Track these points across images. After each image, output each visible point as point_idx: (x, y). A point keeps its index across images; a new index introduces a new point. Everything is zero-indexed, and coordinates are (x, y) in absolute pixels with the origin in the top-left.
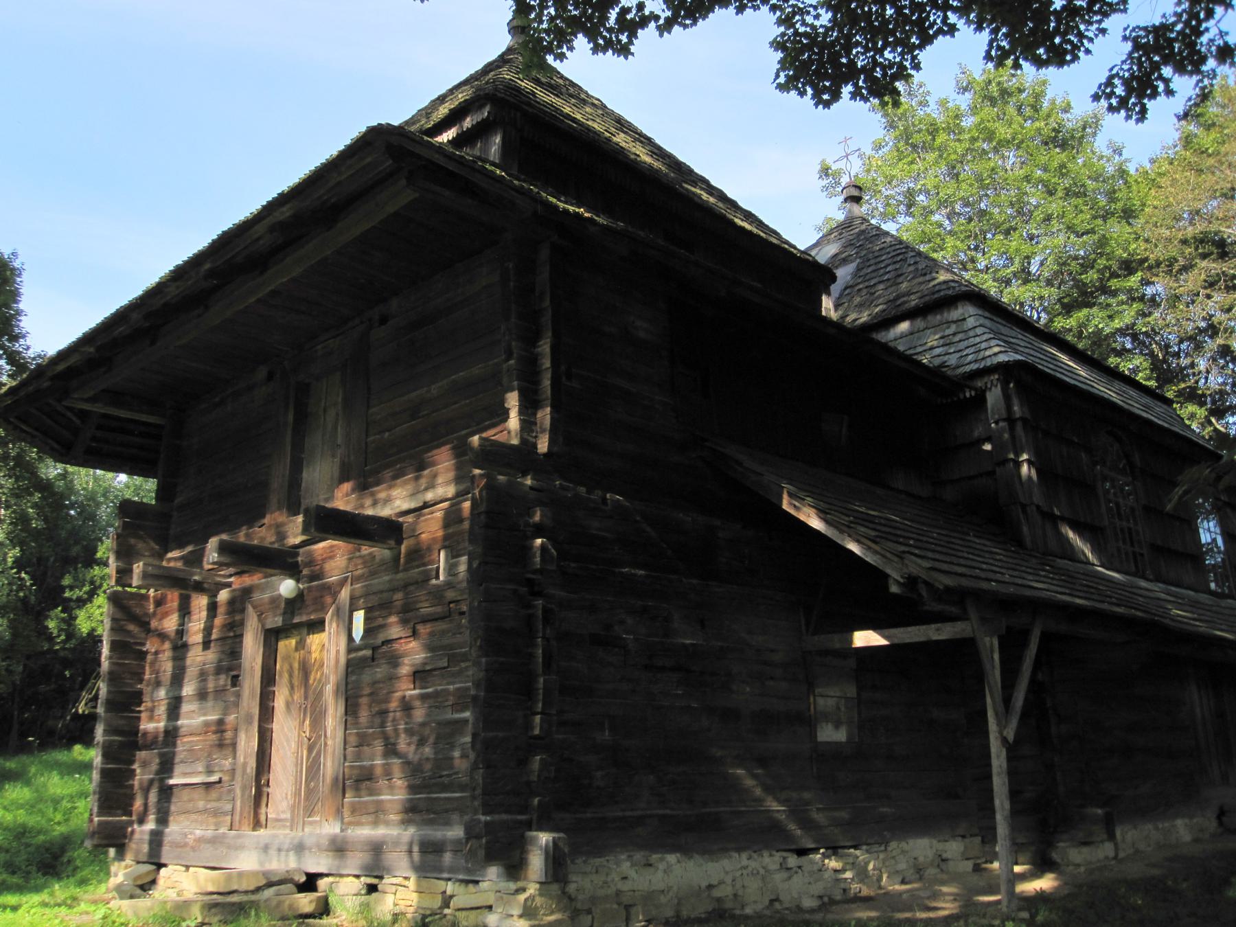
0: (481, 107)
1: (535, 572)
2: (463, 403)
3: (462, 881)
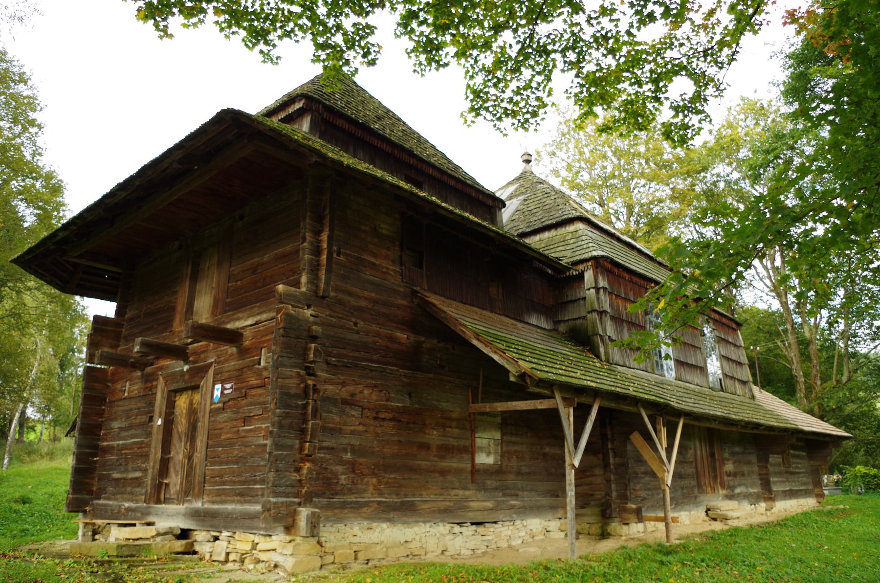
0: (300, 100)
1: (311, 362)
2: (280, 266)
3: (262, 535)
